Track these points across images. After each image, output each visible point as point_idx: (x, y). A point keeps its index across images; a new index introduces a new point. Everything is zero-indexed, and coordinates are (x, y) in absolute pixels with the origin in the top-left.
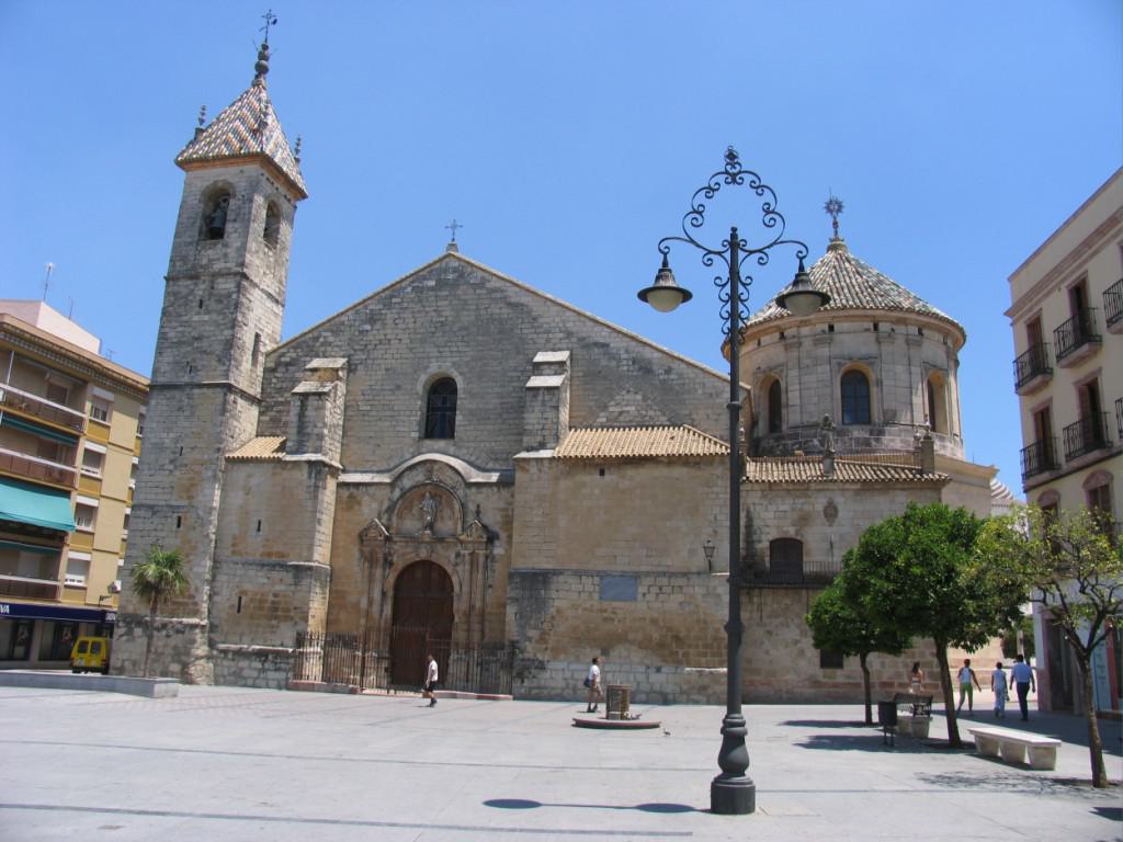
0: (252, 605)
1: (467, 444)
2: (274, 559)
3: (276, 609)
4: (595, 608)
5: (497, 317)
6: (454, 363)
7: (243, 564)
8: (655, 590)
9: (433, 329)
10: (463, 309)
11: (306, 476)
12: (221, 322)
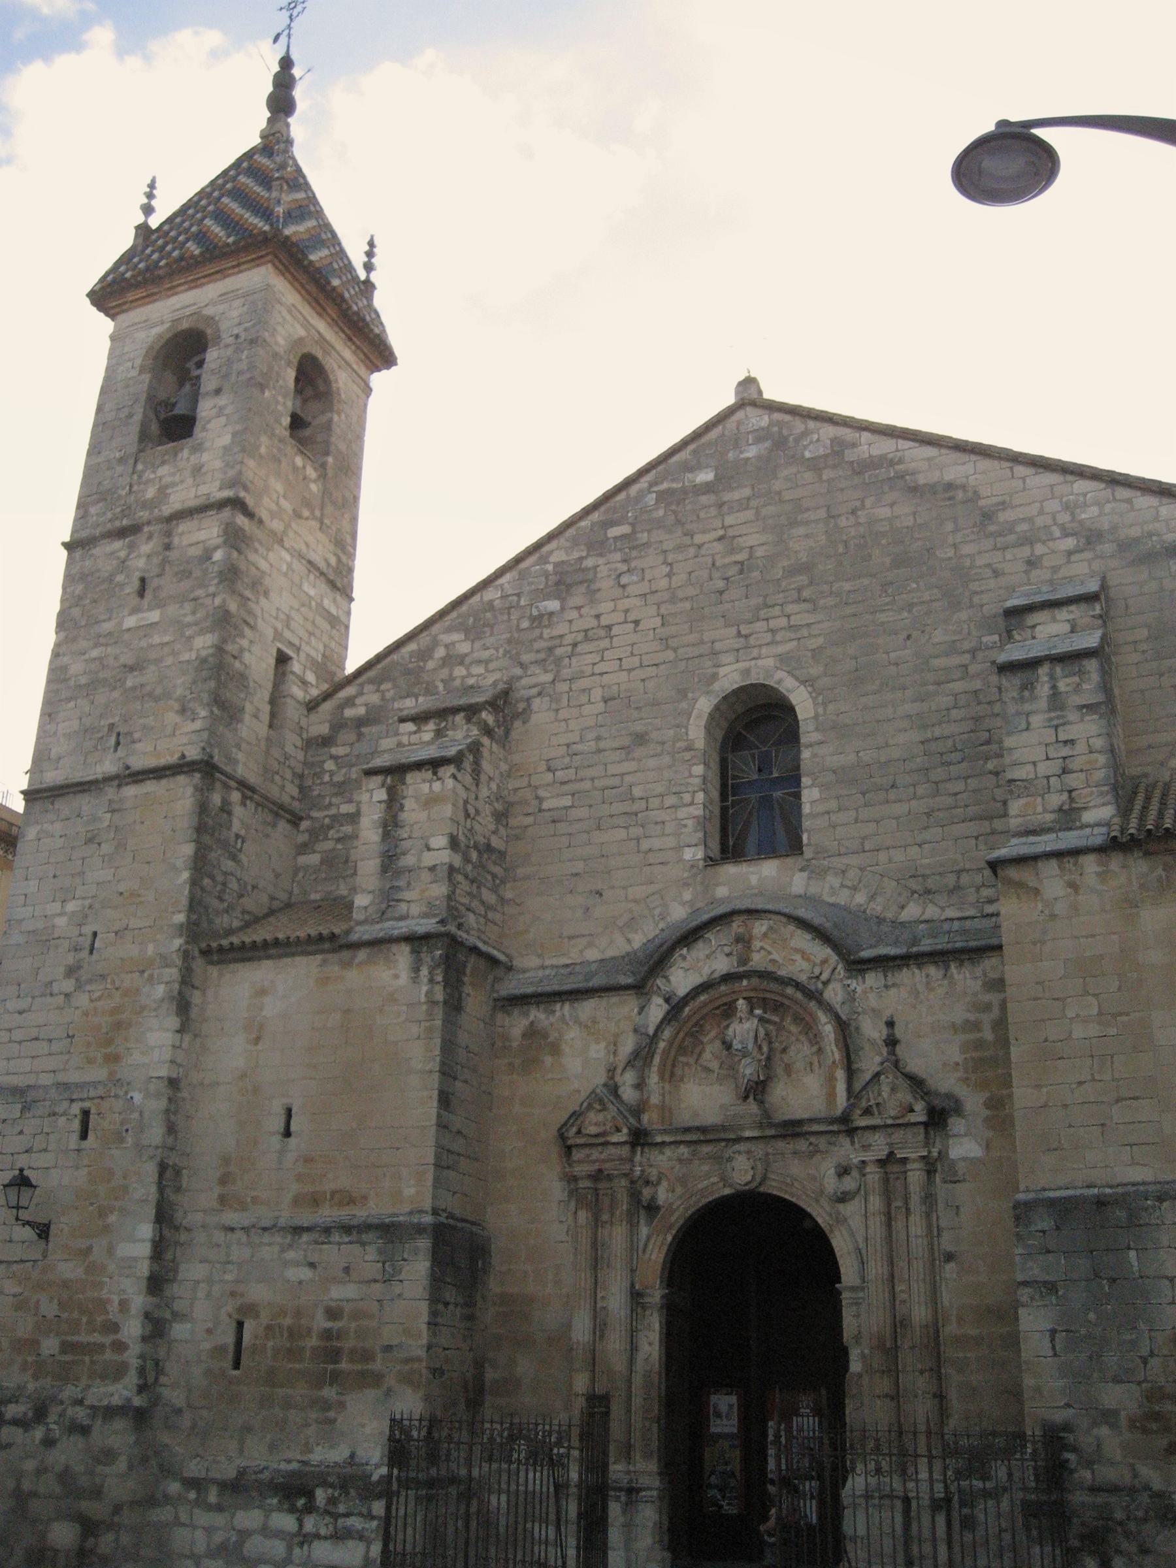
0: (270, 1344)
1: (838, 862)
2: (327, 1214)
3: (334, 1355)
9: (721, 584)
10: (793, 524)
12: (189, 619)
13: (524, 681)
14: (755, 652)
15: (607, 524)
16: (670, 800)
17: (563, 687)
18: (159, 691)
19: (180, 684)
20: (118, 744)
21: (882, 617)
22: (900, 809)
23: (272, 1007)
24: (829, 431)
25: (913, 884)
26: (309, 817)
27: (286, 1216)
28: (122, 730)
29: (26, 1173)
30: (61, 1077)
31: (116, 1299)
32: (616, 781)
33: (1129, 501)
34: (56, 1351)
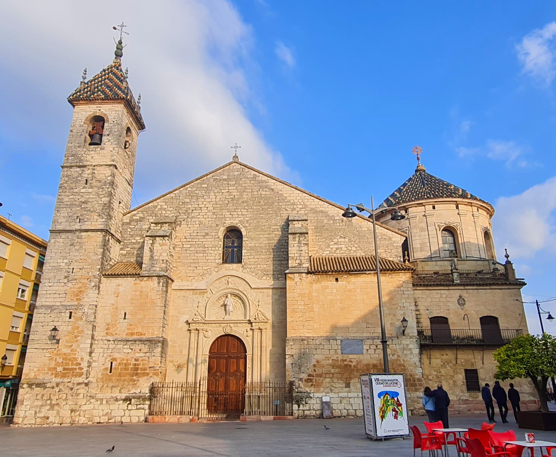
0: (120, 367)
1: (250, 266)
2: (135, 337)
4: (339, 359)
5: (263, 196)
6: (240, 221)
7: (114, 341)
8: (373, 347)
9: (227, 202)
10: (244, 191)
11: (156, 284)
12: (101, 193)
13: (180, 217)
14: (234, 219)
15: (201, 184)
16: (213, 249)
17: (189, 220)
18: (92, 210)
19: (99, 208)
20: (80, 221)
21: (262, 216)
22: (263, 257)
23: (121, 289)
24: (253, 172)
25: (265, 273)
26: (123, 242)
27: (124, 337)
28: (81, 218)
29: (56, 327)
30: (63, 304)
31: (80, 358)
32: (201, 243)
33: (313, 200)
34: (62, 370)
